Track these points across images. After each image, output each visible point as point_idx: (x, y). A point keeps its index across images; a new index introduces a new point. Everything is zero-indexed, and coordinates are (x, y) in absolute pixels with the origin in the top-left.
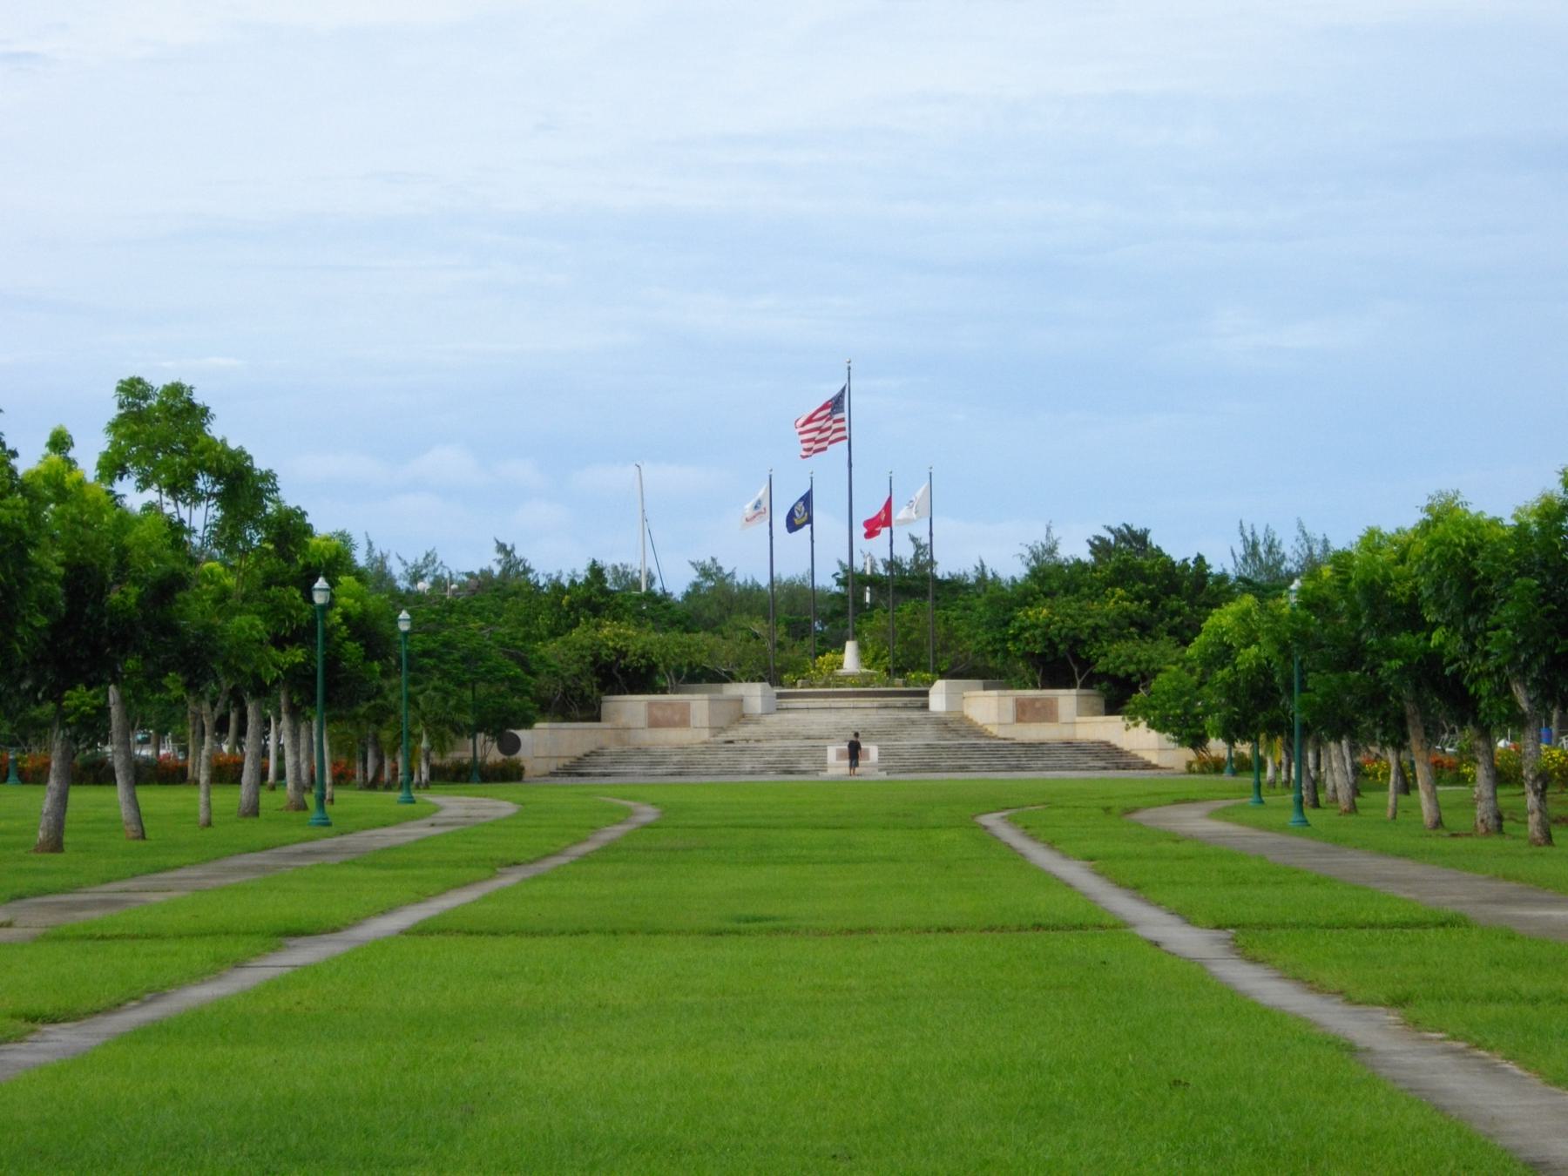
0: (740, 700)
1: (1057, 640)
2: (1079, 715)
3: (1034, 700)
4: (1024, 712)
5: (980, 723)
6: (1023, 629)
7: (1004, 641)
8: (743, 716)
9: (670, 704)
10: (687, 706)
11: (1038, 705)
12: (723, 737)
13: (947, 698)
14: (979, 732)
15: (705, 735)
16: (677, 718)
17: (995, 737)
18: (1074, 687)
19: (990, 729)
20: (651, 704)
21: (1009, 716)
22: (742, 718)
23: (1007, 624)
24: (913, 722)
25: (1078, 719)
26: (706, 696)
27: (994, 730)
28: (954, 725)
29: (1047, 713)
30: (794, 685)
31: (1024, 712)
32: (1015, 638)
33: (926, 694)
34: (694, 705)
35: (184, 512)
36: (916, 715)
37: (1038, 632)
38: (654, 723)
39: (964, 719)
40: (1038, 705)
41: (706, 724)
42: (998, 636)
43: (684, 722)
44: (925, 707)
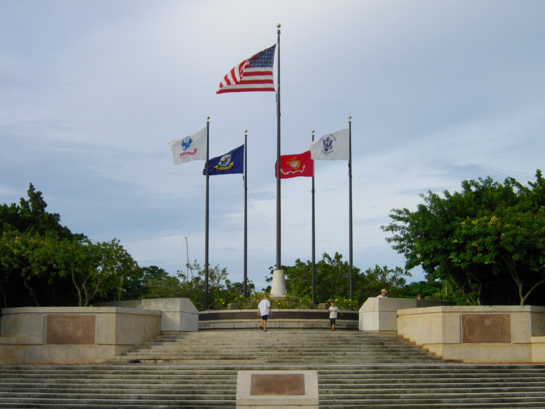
0: (159, 316)
1: (510, 248)
2: (533, 335)
3: (483, 317)
4: (471, 332)
5: (419, 343)
6: (469, 238)
7: (446, 252)
8: (161, 333)
9: (73, 317)
10: (91, 321)
11: (487, 322)
12: (132, 356)
13: (380, 316)
14: (421, 353)
15: (111, 353)
16: (80, 333)
17: (440, 359)
18: (518, 303)
19: (432, 350)
20: (50, 317)
21: (456, 336)
22: (160, 334)
23: (449, 234)
24: (346, 342)
25: (533, 339)
26: (113, 309)
27: (439, 352)
28: (390, 344)
29: (499, 333)
30: (225, 307)
31: (471, 332)
32: (460, 248)
33: (356, 317)
34: (99, 319)
35: (95, 292)
36: (348, 334)
37: (488, 239)
38: (55, 338)
39: (399, 339)
40: (487, 322)
41: (112, 339)
42: (439, 246)
43: (88, 339)
44: (355, 328)
